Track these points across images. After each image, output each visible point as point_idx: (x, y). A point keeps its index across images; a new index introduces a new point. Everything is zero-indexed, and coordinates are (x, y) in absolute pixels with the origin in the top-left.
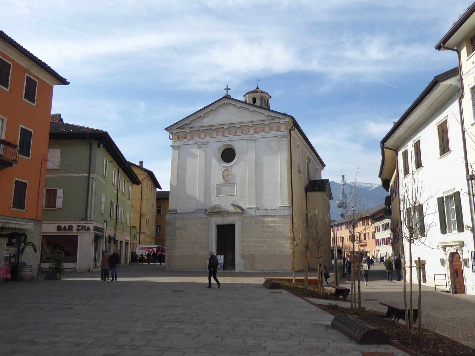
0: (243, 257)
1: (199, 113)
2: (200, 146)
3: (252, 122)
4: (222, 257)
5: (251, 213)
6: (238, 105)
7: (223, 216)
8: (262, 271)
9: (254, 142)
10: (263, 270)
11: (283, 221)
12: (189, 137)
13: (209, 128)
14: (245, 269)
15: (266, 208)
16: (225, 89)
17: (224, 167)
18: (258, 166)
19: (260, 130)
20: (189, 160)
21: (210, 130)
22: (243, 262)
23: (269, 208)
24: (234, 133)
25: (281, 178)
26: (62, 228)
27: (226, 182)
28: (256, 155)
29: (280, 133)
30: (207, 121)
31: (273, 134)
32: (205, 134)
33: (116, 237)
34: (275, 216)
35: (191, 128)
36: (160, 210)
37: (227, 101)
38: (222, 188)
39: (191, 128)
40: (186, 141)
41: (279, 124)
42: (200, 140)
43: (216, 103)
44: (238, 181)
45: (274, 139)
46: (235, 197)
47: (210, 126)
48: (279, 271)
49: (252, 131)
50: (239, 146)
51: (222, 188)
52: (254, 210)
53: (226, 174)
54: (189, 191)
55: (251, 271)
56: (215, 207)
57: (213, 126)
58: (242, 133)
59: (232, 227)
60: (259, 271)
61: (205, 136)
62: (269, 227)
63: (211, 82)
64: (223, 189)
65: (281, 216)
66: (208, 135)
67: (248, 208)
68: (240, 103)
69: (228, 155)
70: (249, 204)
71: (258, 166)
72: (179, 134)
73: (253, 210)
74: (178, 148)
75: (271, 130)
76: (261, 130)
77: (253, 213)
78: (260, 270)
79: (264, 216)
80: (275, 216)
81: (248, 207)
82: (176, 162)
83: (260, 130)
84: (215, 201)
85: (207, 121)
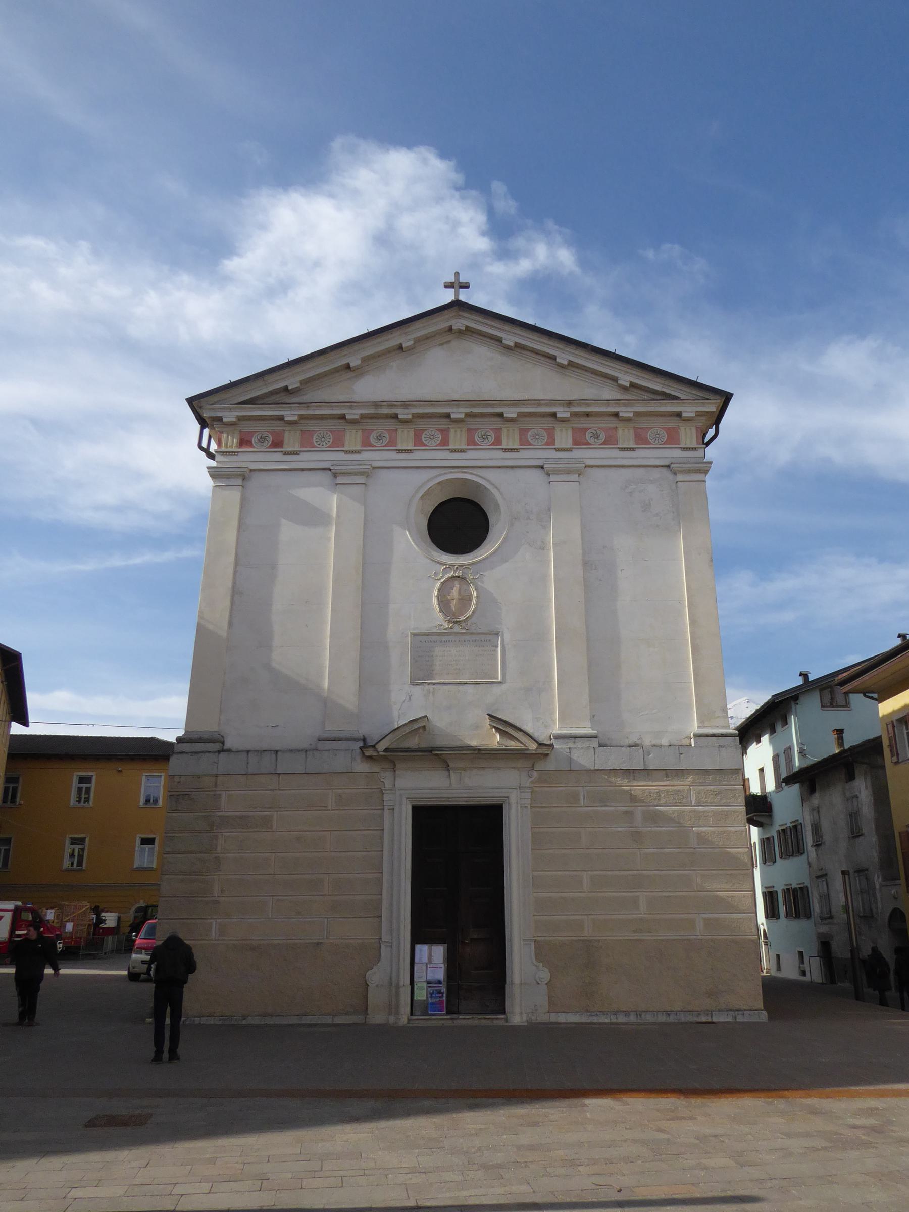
0: (542, 952)
1: (345, 351)
2: (340, 480)
3: (569, 403)
4: (439, 952)
5: (575, 756)
6: (510, 339)
7: (447, 767)
8: (633, 1018)
9: (574, 477)
10: (638, 1014)
11: (718, 793)
12: (292, 440)
13: (385, 411)
14: (553, 1005)
15: (633, 739)
16: (448, 286)
17: (450, 567)
18: (594, 574)
19: (596, 436)
20: (289, 531)
21: (390, 420)
23: (648, 741)
24: (491, 439)
25: (693, 622)
27: (457, 629)
28: (583, 527)
29: (677, 454)
30: (373, 388)
31: (646, 455)
32: (366, 433)
33: (175, 756)
34: (680, 773)
35: (308, 405)
36: (15, 790)
37: (459, 323)
38: (438, 651)
39: (308, 405)
41: (673, 423)
42: (341, 456)
43: (419, 324)
44: (509, 624)
45: (656, 474)
46: (496, 690)
47: (391, 404)
48: (710, 1013)
49: (564, 438)
50: (508, 484)
51: (438, 651)
52: (587, 743)
53: (455, 593)
54: (284, 656)
55: (584, 1019)
56: (419, 726)
57: (405, 404)
58: (524, 442)
59: (487, 821)
60: (622, 1019)
61: (366, 443)
62: (654, 818)
63: (119, 509)
64: (444, 654)
65: (706, 772)
66: (379, 438)
67: (557, 737)
68: (518, 330)
69: (458, 524)
70: (562, 718)
71: (594, 574)
72: (247, 427)
73: (580, 744)
74: (239, 481)
75: (641, 440)
76: (603, 436)
77: (583, 757)
78: (627, 1013)
79: (630, 773)
80: (680, 773)
81: (556, 729)
82: (231, 536)
83: (596, 436)
84: (405, 703)
85: (373, 388)
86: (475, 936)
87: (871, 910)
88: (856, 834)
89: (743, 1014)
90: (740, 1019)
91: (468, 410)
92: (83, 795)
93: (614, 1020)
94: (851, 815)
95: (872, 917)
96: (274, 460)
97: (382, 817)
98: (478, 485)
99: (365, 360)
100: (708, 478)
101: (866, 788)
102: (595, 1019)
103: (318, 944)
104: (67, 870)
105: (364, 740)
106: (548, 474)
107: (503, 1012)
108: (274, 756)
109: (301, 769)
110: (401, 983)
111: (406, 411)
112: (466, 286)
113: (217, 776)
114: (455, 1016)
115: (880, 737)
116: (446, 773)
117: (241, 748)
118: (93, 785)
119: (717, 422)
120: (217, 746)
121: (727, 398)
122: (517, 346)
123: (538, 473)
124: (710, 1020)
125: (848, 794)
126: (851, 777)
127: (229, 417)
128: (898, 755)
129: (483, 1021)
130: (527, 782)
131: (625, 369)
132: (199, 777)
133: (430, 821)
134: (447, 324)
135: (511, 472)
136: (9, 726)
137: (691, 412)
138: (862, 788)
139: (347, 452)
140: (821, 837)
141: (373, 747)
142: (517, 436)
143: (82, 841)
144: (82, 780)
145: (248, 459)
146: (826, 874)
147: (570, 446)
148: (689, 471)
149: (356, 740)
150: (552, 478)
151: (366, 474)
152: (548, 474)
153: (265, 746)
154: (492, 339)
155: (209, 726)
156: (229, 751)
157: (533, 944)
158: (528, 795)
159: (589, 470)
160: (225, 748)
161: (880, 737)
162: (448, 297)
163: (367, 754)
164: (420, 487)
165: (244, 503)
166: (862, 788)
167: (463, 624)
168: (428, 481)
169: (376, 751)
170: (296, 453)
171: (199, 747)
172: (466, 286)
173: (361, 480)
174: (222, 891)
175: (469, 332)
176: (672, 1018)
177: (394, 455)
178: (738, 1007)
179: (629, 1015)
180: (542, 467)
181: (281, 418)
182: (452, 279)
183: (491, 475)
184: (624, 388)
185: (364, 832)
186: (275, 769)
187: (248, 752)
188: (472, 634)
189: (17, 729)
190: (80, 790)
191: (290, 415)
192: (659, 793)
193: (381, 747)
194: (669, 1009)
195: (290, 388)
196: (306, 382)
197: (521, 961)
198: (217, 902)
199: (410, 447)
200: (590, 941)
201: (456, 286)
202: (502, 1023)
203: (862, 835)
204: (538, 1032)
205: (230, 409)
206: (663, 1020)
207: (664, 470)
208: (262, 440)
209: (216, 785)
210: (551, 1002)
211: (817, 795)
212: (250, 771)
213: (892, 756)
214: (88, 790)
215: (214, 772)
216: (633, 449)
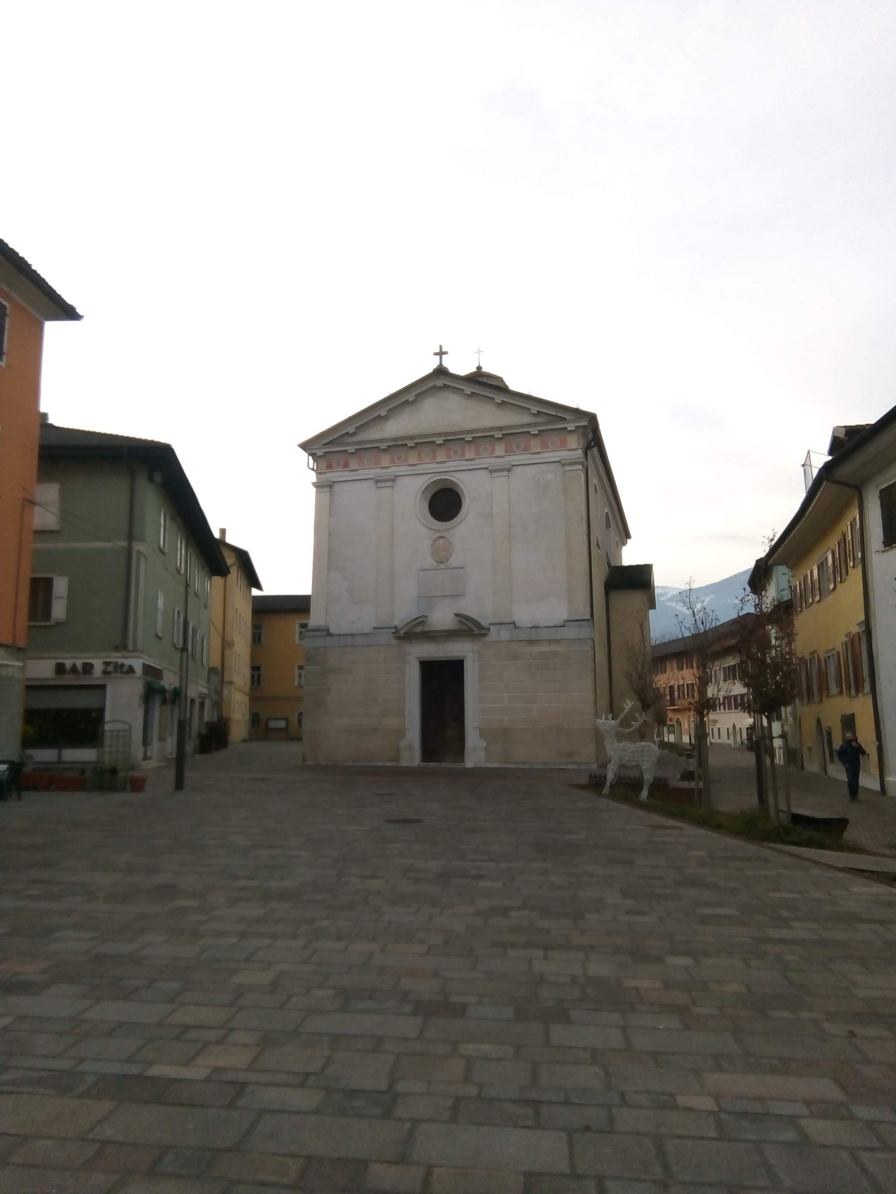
3: (500, 429)
9: (506, 473)
12: (353, 464)
17: (436, 531)
21: (399, 446)
30: (395, 427)
37: (439, 382)
45: (553, 467)
74: (328, 489)
85: (395, 427)
96: (344, 475)
133: (429, 668)
136: (250, 591)
145: (332, 476)
147: (503, 454)
151: (393, 480)
158: (476, 655)
173: (389, 484)
175: (446, 386)
177: (464, 463)
182: (438, 351)
189: (255, 592)
191: (351, 449)
197: (472, 738)
204: (479, 773)
205: (320, 448)
208: (338, 464)
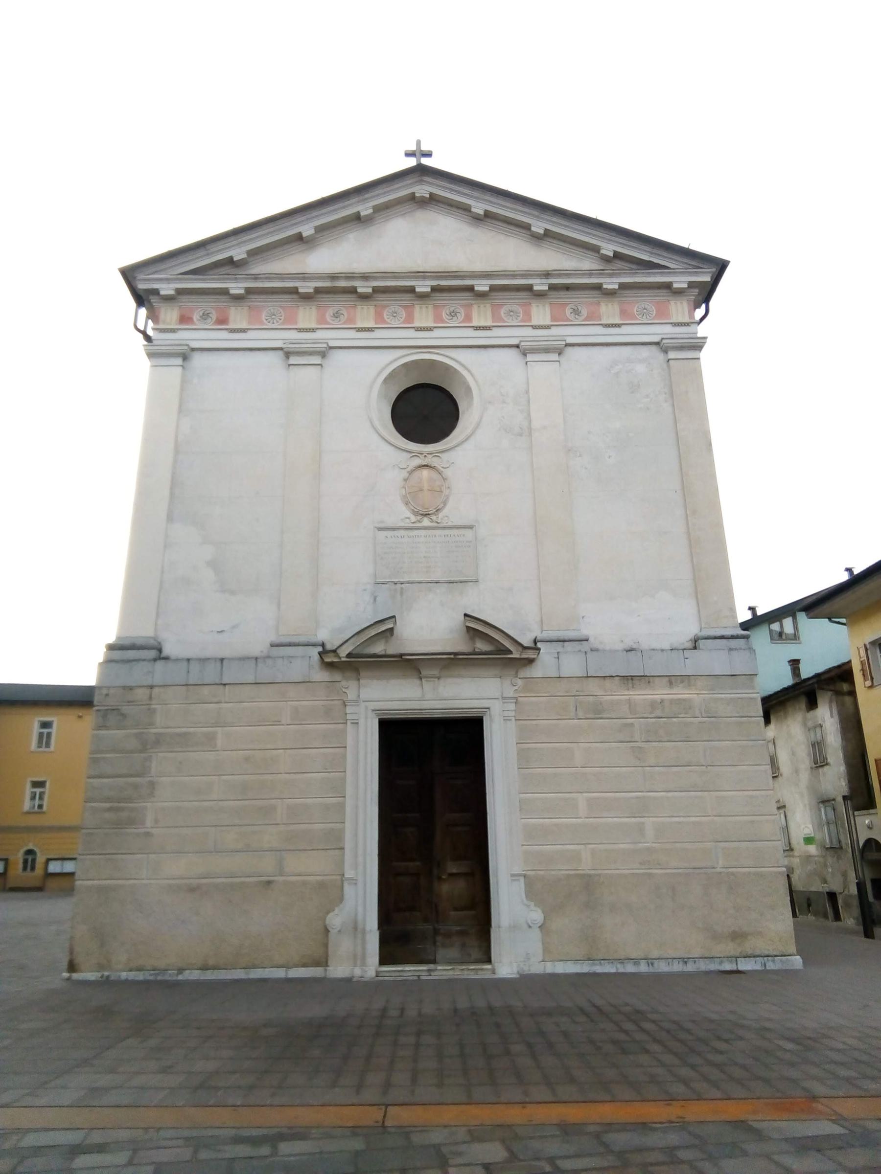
0: (534, 889)
1: (299, 218)
2: (293, 360)
3: (547, 275)
8: (643, 968)
10: (650, 961)
13: (342, 284)
14: (548, 953)
16: (409, 154)
22: (537, 916)
26: (643, 963)
27: (426, 522)
34: (686, 679)
35: (256, 277)
37: (422, 190)
39: (256, 277)
40: (224, 335)
47: (350, 277)
57: (365, 277)
59: (462, 738)
60: (630, 968)
74: (179, 361)
78: (636, 962)
86: (454, 871)
87: (840, 842)
88: (819, 762)
89: (773, 961)
90: (771, 966)
91: (435, 283)
92: (44, 740)
93: (621, 970)
94: (813, 745)
95: (841, 848)
97: (344, 732)
98: (448, 368)
99: (320, 229)
100: (704, 354)
101: (832, 716)
102: (599, 969)
103: (269, 883)
104: (28, 813)
105: (323, 645)
106: (525, 355)
107: (489, 961)
108: (219, 664)
109: (251, 679)
110: (368, 928)
111: (366, 284)
112: (428, 155)
113: (151, 687)
114: (432, 966)
115: (850, 662)
116: (418, 682)
117: (180, 656)
118: (54, 730)
119: (707, 300)
120: (153, 654)
121: (721, 266)
122: (488, 215)
123: (513, 352)
124: (735, 968)
125: (810, 724)
126: (812, 704)
127: (167, 289)
128: (872, 679)
129: (466, 972)
130: (510, 692)
131: (607, 236)
132: (131, 688)
133: (402, 739)
134: (410, 191)
135: (482, 352)
137: (684, 282)
138: (826, 716)
139: (300, 330)
140: (778, 769)
141: (334, 651)
142: (489, 313)
143: (40, 784)
144: (45, 725)
146: (784, 807)
147: (548, 322)
148: (681, 348)
149: (314, 645)
150: (530, 357)
151: (323, 354)
152: (525, 355)
153: (208, 654)
154: (458, 208)
155: (144, 631)
156: (166, 658)
157: (522, 880)
159: (569, 349)
160: (163, 655)
161: (850, 662)
162: (412, 162)
163: (328, 660)
164: (384, 369)
165: (184, 382)
166: (826, 716)
167: (434, 518)
168: (391, 362)
169: (338, 656)
170: (244, 331)
171: (131, 654)
172: (428, 155)
173: (316, 360)
174: (156, 821)
175: (433, 200)
176: (690, 968)
178: (767, 953)
179: (639, 964)
180: (517, 346)
181: (225, 292)
182: (414, 148)
183: (463, 356)
184: (606, 259)
185: (322, 750)
186: (221, 679)
187: (188, 660)
188: (444, 528)
190: (41, 735)
192: (662, 701)
193: (343, 652)
194: (686, 956)
195: (235, 259)
196: (252, 253)
197: (509, 901)
198: (148, 834)
199: (371, 324)
200: (590, 876)
201: (417, 154)
202: (488, 976)
203: (827, 764)
205: (168, 280)
206: (680, 970)
207: (654, 348)
208: (205, 316)
209: (150, 698)
210: (546, 950)
211: (772, 726)
212: (191, 682)
213: (865, 680)
214: (49, 735)
215: (149, 682)
216: (618, 326)
